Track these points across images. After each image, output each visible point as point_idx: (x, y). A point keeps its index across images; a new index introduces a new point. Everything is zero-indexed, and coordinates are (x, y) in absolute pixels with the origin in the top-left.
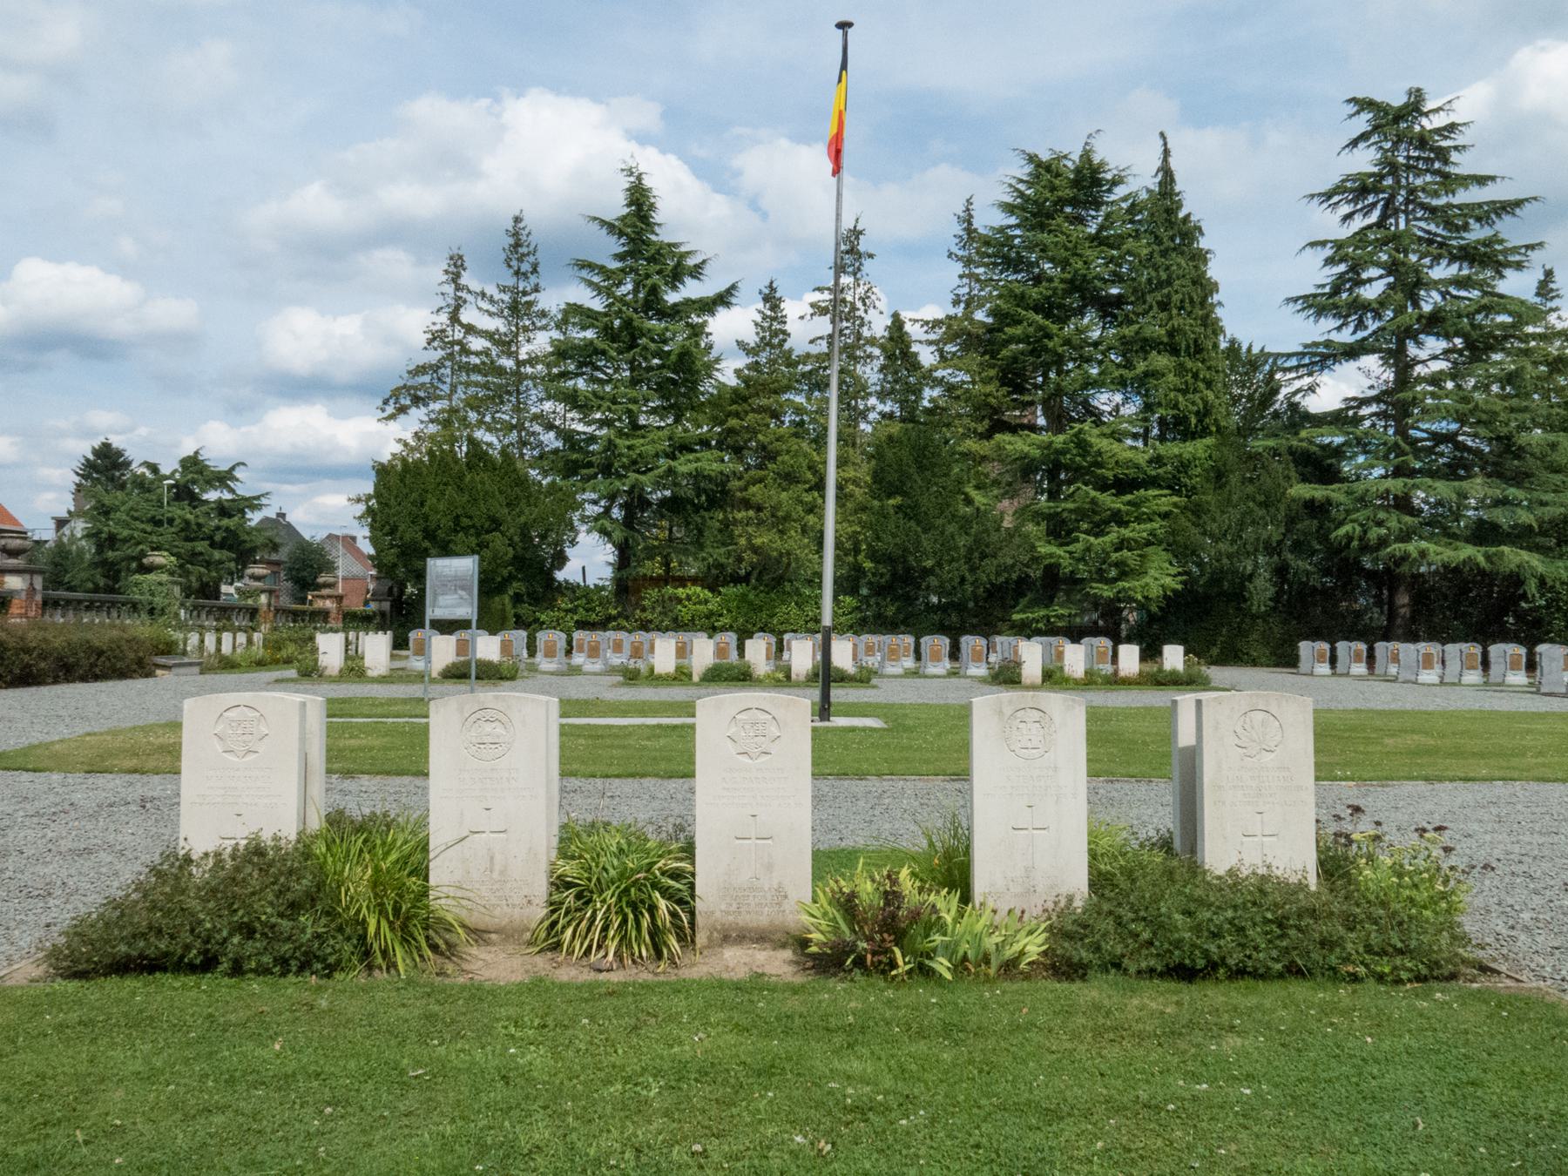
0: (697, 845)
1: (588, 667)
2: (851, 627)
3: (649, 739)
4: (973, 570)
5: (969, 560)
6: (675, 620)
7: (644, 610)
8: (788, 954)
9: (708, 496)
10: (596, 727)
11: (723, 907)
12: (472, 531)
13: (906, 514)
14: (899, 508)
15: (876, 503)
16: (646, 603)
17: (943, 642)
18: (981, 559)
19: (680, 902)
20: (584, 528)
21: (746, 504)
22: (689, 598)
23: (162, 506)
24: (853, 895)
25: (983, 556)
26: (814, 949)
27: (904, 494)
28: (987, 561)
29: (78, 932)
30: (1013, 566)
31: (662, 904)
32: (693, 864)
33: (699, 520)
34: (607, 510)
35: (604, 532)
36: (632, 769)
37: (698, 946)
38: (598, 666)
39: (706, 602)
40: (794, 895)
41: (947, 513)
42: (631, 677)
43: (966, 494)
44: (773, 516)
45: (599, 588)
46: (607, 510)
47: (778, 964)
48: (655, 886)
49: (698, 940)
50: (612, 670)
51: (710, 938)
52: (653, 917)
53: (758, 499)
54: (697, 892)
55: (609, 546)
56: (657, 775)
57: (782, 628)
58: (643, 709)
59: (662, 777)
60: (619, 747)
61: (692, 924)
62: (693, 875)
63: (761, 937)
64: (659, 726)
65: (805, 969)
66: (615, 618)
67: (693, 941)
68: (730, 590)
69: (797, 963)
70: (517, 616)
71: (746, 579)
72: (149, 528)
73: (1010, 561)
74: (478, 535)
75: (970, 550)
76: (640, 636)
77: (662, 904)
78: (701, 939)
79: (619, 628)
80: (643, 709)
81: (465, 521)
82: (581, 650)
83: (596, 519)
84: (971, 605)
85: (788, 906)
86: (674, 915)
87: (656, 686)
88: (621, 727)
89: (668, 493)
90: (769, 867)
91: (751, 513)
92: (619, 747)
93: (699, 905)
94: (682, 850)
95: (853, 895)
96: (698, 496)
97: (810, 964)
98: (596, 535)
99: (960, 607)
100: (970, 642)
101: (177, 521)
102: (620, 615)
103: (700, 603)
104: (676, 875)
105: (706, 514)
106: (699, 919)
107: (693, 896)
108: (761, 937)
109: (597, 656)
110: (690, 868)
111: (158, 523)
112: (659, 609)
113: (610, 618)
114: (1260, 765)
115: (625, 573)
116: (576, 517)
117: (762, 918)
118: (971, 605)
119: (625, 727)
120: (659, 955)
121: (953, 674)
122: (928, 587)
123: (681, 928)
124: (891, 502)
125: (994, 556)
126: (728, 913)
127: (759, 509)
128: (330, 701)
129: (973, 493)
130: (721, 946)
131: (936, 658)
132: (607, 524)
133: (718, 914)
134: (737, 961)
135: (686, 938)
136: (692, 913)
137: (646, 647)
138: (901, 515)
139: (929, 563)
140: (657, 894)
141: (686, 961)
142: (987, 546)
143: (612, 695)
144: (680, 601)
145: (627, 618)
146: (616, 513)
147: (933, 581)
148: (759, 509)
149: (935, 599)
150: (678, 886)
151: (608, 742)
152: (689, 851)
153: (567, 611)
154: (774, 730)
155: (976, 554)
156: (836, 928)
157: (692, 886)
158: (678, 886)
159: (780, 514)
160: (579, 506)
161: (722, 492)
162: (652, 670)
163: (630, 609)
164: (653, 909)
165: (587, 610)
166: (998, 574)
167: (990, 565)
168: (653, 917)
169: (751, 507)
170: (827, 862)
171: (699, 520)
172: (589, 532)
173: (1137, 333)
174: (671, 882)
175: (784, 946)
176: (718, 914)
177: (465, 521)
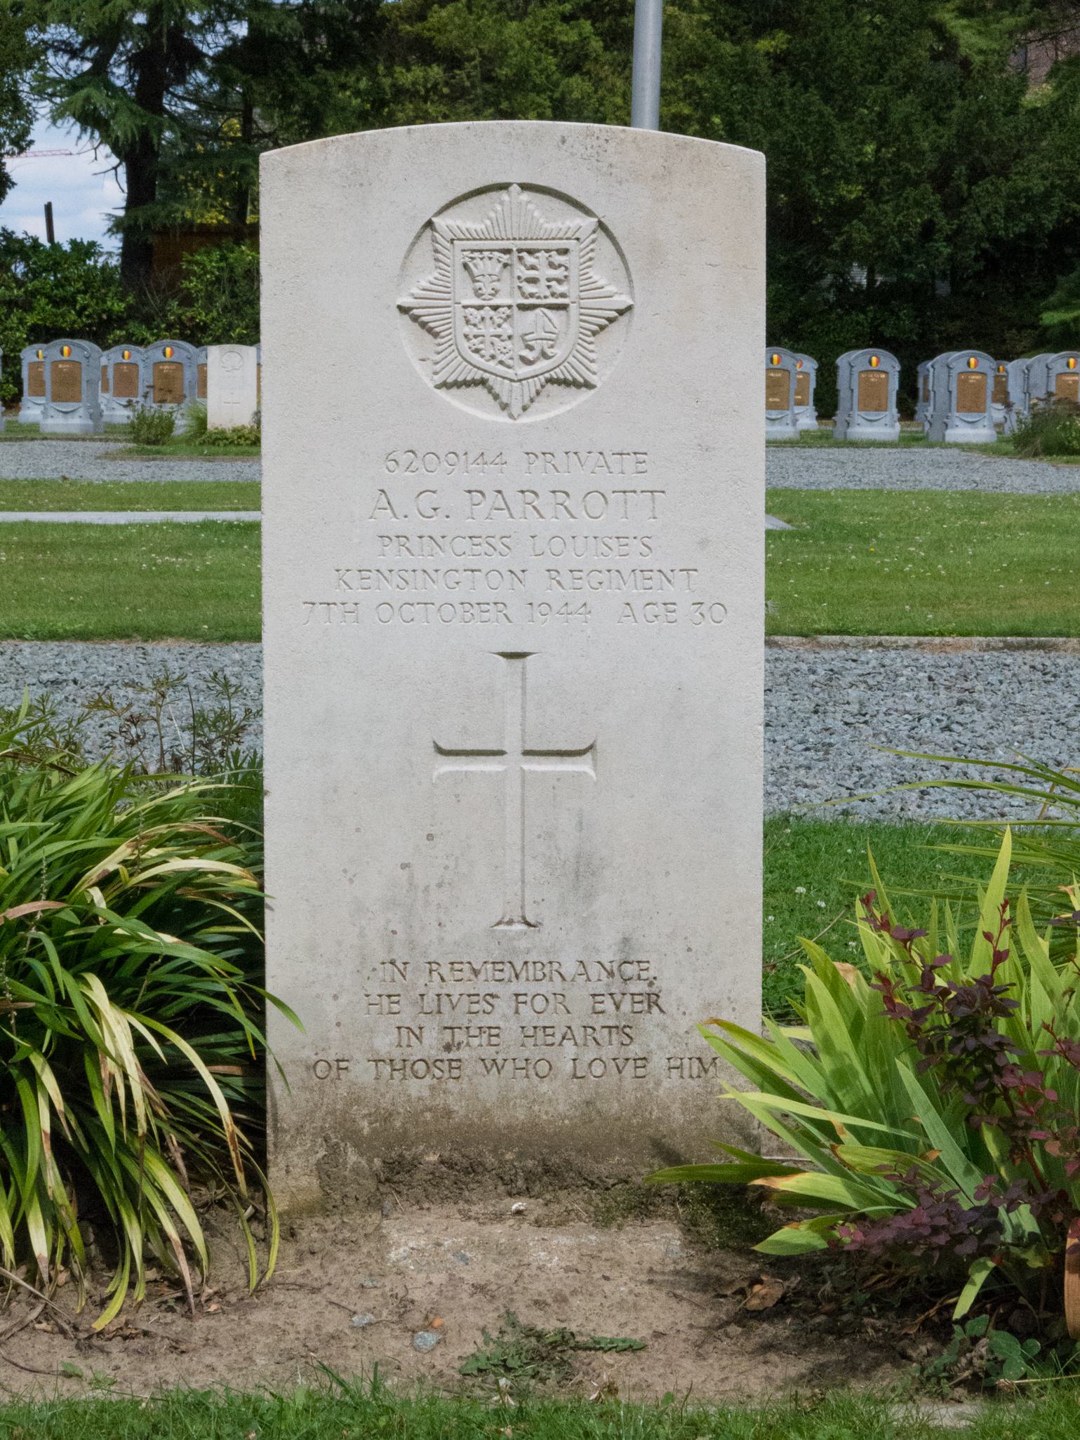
0: (271, 779)
1: (56, 422)
3: (177, 551)
4: (954, 205)
5: (941, 180)
7: (187, 301)
8: (661, 1242)
9: (332, 35)
10: (56, 526)
11: (385, 1043)
13: (796, 74)
14: (779, 60)
15: (727, 48)
16: (192, 284)
17: (886, 365)
18: (972, 181)
19: (200, 1021)
20: (43, 108)
21: (426, 51)
24: (988, 1000)
25: (977, 174)
26: (795, 1236)
27: (792, 26)
28: (985, 184)
30: (1047, 195)
31: (117, 1030)
32: (254, 862)
33: (315, 91)
34: (100, 66)
35: (90, 119)
36: (124, 617)
37: (279, 1203)
38: (77, 422)
40: (685, 993)
41: (895, 70)
42: (150, 437)
43: (939, 30)
44: (488, 78)
45: (84, 250)
46: (100, 66)
47: (620, 1285)
48: (80, 956)
49: (276, 1179)
50: (103, 431)
51: (326, 1171)
52: (77, 1091)
53: (452, 38)
54: (276, 980)
55: (106, 149)
56: (190, 634)
58: (170, 497)
59: (206, 639)
60: (95, 568)
61: (252, 1108)
62: (255, 907)
63: (548, 1169)
64: (207, 526)
65: (746, 1318)
66: (120, 321)
67: (255, 1182)
69: (709, 1285)
73: (1038, 186)
75: (947, 161)
76: (170, 351)
77: (117, 1030)
78: (290, 1176)
79: (130, 339)
80: (170, 497)
82: (38, 391)
83: (73, 86)
84: (943, 288)
85: (656, 1038)
86: (166, 1073)
87: (211, 457)
88: (105, 528)
89: (241, 30)
90: (583, 874)
91: (436, 71)
92: (95, 568)
93: (281, 1039)
94: (209, 803)
95: (988, 1000)
96: (311, 36)
97: (767, 1292)
98: (71, 126)
99: (918, 295)
100: (953, 368)
102: (132, 313)
104: (179, 909)
105: (330, 76)
106: (283, 1096)
107: (255, 1000)
108: (548, 1169)
109: (75, 398)
110: (240, 879)
112: (223, 299)
115: (142, 215)
116: (25, 83)
117: (549, 1091)
118: (943, 288)
119: (118, 527)
120: (110, 1245)
121: (908, 441)
122: (847, 246)
123: (207, 1128)
124: (764, 45)
125: (1003, 171)
126: (404, 1067)
127: (453, 61)
128: (962, 408)
129: (955, 24)
130: (374, 1203)
131: (872, 403)
132: (100, 99)
133: (362, 1073)
134: (441, 1280)
135: (229, 1167)
136: (254, 1064)
137: (189, 374)
138: (785, 76)
139: (852, 192)
140: (98, 992)
141: (227, 1272)
142: (987, 150)
143: (97, 474)
146: (119, 74)
147: (859, 232)
148: (453, 61)
149: (859, 276)
150: (189, 953)
151: (70, 557)
152: (239, 815)
154: (605, 282)
155: (961, 170)
156: (902, 1141)
157: (251, 957)
158: (189, 953)
159: (503, 72)
160: (33, 56)
161: (363, 27)
162: (202, 422)
163: (154, 301)
164: (75, 1057)
165: (56, 303)
166: (1010, 214)
167: (990, 198)
168: (77, 1091)
169: (438, 59)
170: (807, 865)
171: (315, 91)
172: (56, 116)
174: (167, 941)
175: (643, 1205)
176: (362, 1073)
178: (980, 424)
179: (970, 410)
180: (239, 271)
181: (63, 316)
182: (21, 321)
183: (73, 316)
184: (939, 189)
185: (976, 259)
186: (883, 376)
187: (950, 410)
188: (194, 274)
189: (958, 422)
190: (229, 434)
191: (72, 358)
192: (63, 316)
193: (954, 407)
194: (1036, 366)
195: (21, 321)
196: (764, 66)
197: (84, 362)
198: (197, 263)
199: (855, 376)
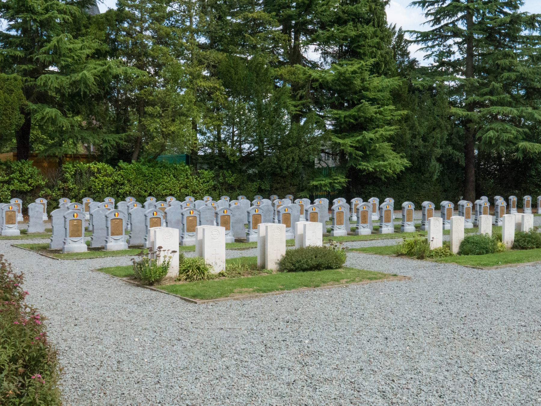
2: (208, 191)
22: (99, 172)
57: (164, 192)
103: (106, 175)
144: (92, 174)
165: (21, 183)
192: (23, 186)
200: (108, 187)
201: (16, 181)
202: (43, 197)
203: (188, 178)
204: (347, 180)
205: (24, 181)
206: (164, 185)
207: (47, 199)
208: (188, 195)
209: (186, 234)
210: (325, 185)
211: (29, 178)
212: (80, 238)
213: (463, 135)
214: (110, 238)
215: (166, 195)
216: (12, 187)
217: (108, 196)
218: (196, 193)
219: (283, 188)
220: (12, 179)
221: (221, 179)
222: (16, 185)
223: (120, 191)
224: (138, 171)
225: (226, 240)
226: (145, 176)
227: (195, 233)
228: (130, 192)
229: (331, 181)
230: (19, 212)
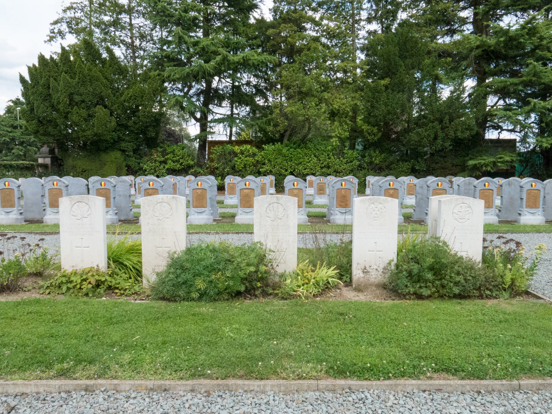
2: (352, 171)
6: (233, 168)
12: (83, 105)
22: (242, 153)
23: (17, 120)
29: (405, 213)
39: (254, 155)
57: (305, 172)
68: (269, 148)
70: (128, 166)
71: (281, 140)
72: (10, 130)
74: (88, 108)
81: (77, 98)
101: (23, 127)
103: (249, 156)
111: (15, 127)
113: (190, 167)
114: (461, 218)
124: (383, 82)
128: (528, 206)
144: (236, 154)
145: (201, 166)
153: (161, 162)
165: (174, 162)
173: (541, 72)
177: (77, 98)
178: (537, 214)
179: (531, 208)
180: (227, 152)
181: (176, 165)
182: (164, 167)
183: (179, 166)
184: (440, 124)
185: (450, 146)
186: (491, 191)
187: (522, 208)
188: (214, 153)
189: (526, 213)
190: (77, 279)
191: (106, 187)
192: (176, 165)
193: (524, 206)
194: (548, 185)
195: (164, 167)
196: (383, 88)
197: (112, 189)
198: (215, 150)
199: (478, 192)
200: (250, 166)
201: (170, 161)
202: (192, 175)
203: (329, 158)
204: (519, 158)
205: (176, 161)
206: (305, 164)
207: (285, 176)
208: (330, 175)
209: (193, 210)
210: (487, 165)
211: (180, 158)
212: (491, 209)
213: (261, 21)
214: (525, 210)
215: (308, 175)
216: (167, 167)
217: (250, 174)
218: (340, 173)
219: (443, 168)
220: (167, 159)
221: (367, 159)
222: (170, 165)
223: (261, 170)
224: (280, 152)
225: (299, 219)
226: (285, 156)
227: (348, 209)
228: (271, 171)
229: (494, 160)
230: (271, 187)
